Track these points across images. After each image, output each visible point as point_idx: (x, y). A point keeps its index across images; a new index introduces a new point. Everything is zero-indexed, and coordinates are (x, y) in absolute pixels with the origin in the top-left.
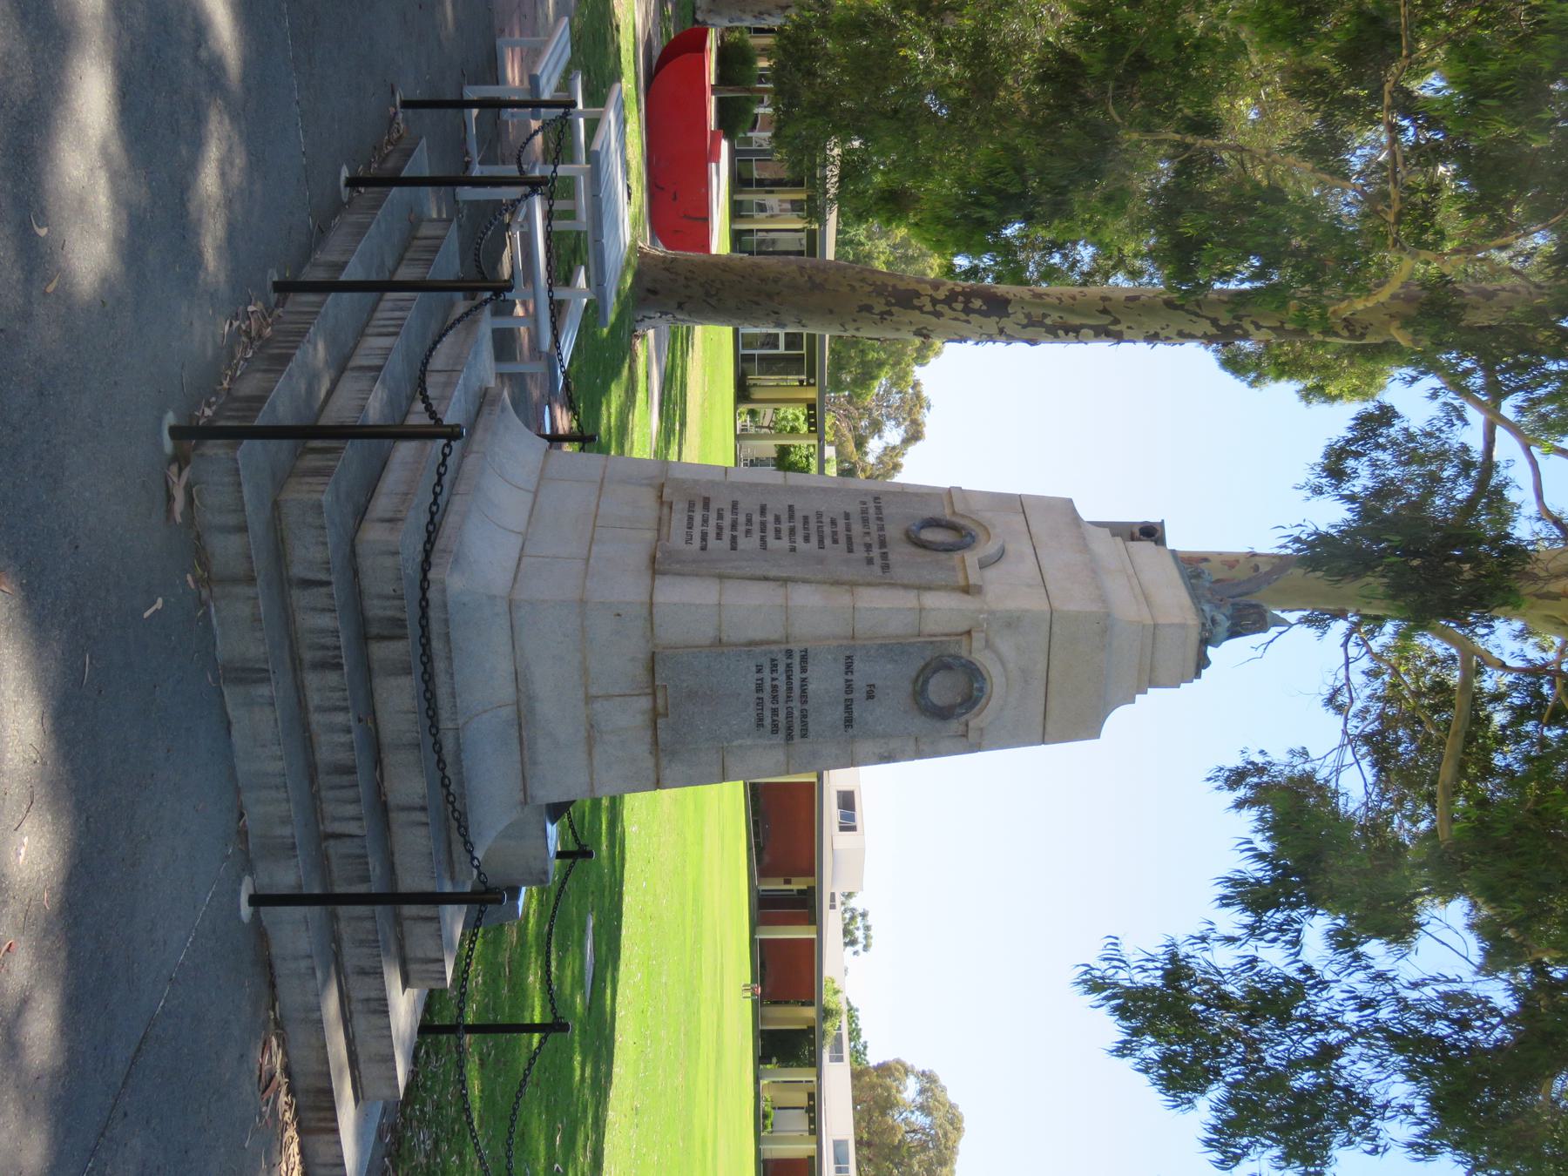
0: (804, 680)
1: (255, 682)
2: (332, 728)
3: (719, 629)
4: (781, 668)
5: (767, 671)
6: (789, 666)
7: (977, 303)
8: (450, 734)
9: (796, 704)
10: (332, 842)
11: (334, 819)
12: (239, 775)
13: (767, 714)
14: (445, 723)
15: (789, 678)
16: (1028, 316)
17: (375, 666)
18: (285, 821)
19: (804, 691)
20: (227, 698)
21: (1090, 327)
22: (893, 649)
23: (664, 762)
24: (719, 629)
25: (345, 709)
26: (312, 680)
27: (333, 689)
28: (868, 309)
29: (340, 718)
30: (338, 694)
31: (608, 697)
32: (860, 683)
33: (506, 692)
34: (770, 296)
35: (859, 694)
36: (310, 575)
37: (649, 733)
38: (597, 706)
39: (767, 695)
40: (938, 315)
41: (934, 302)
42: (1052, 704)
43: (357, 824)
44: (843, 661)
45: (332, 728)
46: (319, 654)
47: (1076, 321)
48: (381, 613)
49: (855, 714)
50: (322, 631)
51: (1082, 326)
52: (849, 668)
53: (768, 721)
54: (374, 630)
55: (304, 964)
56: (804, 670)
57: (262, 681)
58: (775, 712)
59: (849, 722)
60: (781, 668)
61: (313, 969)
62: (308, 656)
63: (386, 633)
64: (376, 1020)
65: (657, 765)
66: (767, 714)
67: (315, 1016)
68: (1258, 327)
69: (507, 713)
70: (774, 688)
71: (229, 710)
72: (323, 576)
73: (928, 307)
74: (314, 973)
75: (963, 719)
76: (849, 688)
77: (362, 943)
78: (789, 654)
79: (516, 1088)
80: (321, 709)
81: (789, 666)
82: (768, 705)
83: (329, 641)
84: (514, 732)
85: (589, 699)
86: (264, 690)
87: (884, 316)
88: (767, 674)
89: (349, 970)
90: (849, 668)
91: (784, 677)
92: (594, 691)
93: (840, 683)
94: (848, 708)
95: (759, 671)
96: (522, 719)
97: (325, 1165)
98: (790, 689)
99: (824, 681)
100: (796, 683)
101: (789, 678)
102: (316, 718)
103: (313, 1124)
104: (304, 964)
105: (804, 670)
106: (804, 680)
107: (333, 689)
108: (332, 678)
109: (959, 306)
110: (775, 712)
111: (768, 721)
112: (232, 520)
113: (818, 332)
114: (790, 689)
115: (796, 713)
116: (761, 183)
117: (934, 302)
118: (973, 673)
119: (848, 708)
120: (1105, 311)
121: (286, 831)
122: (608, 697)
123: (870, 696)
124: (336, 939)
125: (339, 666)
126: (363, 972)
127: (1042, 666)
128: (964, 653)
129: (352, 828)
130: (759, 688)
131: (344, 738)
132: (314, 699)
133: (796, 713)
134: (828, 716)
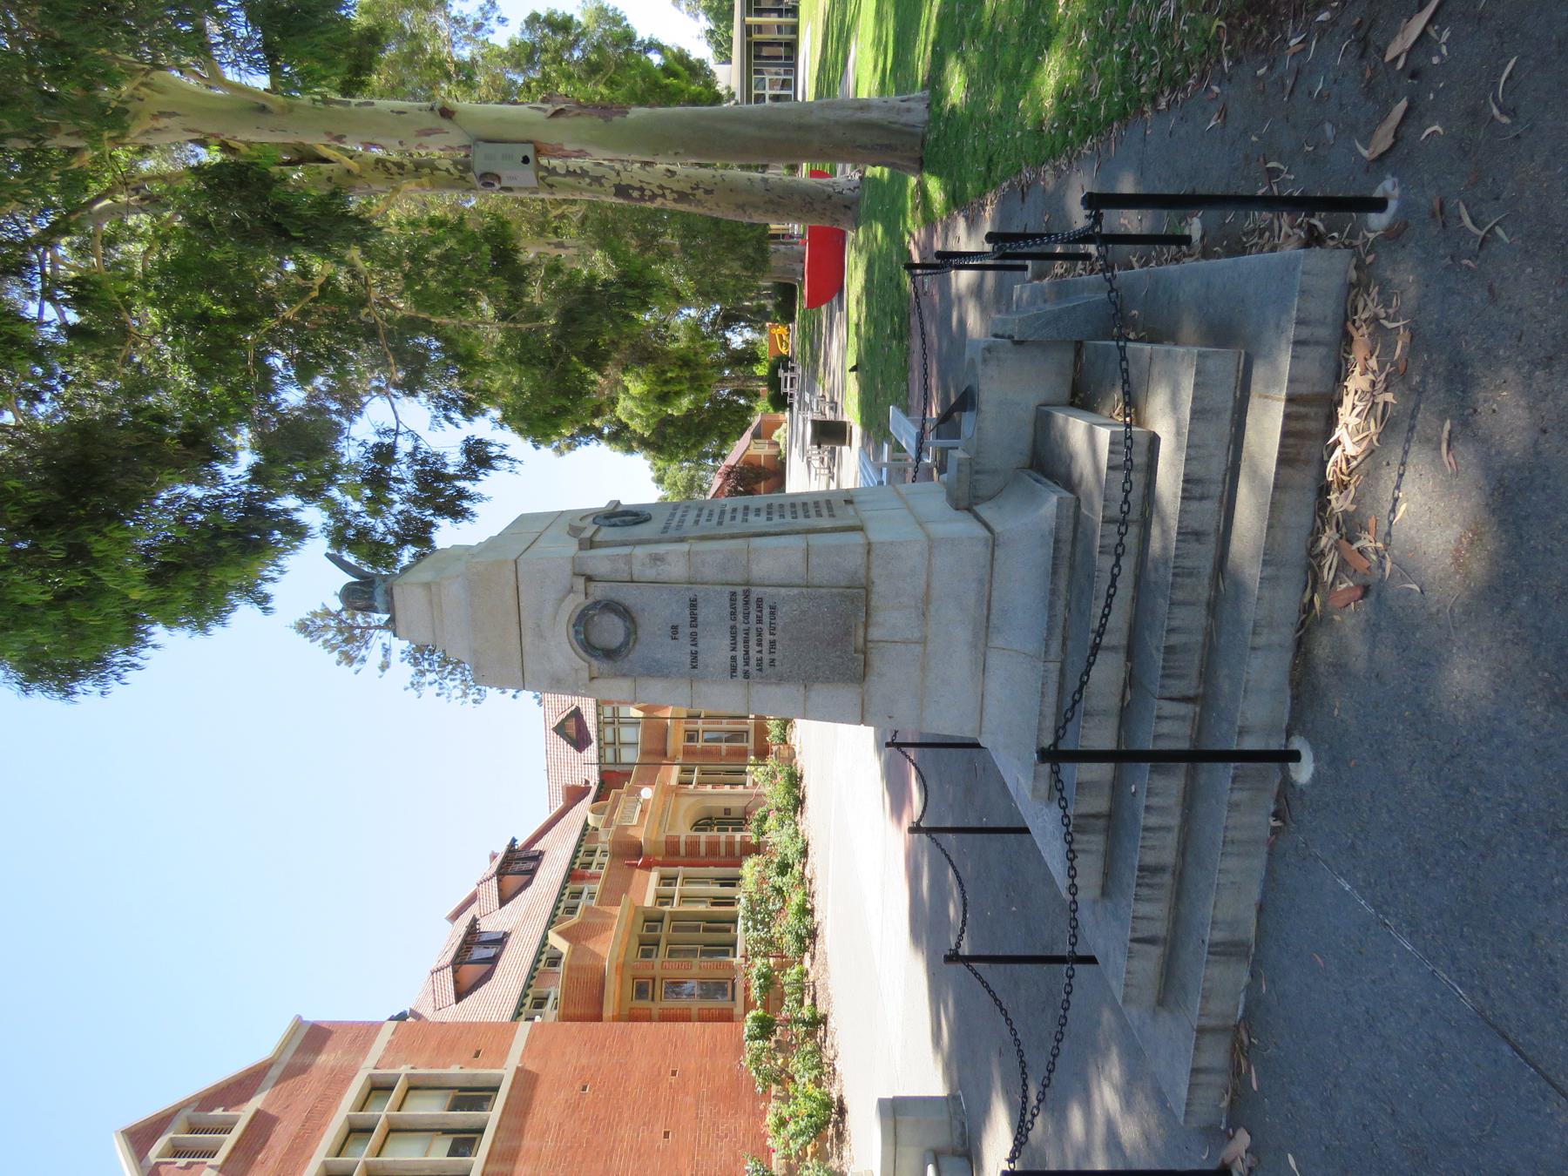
0: (734, 649)
1: (1223, 944)
2: (1161, 810)
3: (806, 699)
4: (753, 662)
5: (766, 662)
6: (747, 664)
7: (636, 194)
8: (1052, 657)
9: (741, 627)
10: (1191, 693)
11: (1183, 718)
12: (1265, 856)
13: (766, 619)
14: (1054, 667)
15: (747, 652)
16: (601, 185)
17: (1107, 790)
18: (1234, 806)
19: (734, 638)
20: (1253, 929)
21: (558, 174)
22: (656, 670)
23: (862, 572)
24: (806, 699)
25: (1146, 829)
26: (1168, 856)
27: (1153, 848)
28: (707, 192)
29: (1153, 821)
30: (1149, 843)
31: (906, 642)
32: (684, 639)
33: (994, 660)
34: (771, 202)
35: (685, 630)
36: (1147, 947)
37: (873, 604)
38: (917, 635)
39: (767, 637)
40: (661, 187)
41: (663, 196)
42: (513, 602)
43: (1164, 713)
44: (700, 665)
45: (1161, 810)
46: (1157, 880)
47: (569, 180)
48: (1093, 838)
49: (687, 612)
50: (1149, 900)
51: (564, 176)
52: (694, 655)
53: (766, 611)
54: (1101, 823)
55: (1261, 641)
56: (734, 658)
57: (1217, 944)
58: (760, 620)
59: (693, 604)
60: (753, 662)
61: (1254, 633)
62: (1167, 879)
63: (1092, 821)
64: (1199, 470)
65: (868, 568)
66: (766, 619)
67: (1270, 571)
68: (447, 170)
69: (997, 641)
70: (760, 644)
71: (1254, 921)
72: (1136, 946)
73: (667, 192)
74: (1255, 626)
75: (590, 600)
76: (694, 638)
77: (1190, 574)
78: (746, 675)
79: (1064, 1045)
80: (1168, 829)
81: (747, 664)
82: (765, 627)
83: (1145, 891)
84: (994, 619)
85: (923, 641)
86: (1219, 936)
87: (697, 187)
88: (766, 657)
89: (1213, 539)
90: (694, 655)
91: (752, 653)
92: (918, 649)
93: (701, 642)
94: (694, 618)
95: (773, 661)
96: (985, 627)
97: (1317, 343)
98: (746, 641)
99: (716, 648)
100: (740, 646)
101: (747, 652)
102: (1174, 821)
103: (1312, 411)
104: (1261, 641)
105: (734, 658)
106: (734, 649)
107: (1153, 848)
108: (1150, 859)
109: (647, 193)
110: (760, 620)
111: (766, 611)
112: (1202, 1078)
113: (745, 106)
114: (746, 641)
115: (740, 617)
116: (780, 44)
117: (663, 196)
118: (589, 647)
119: (694, 618)
120: (551, 186)
121: (1237, 796)
122: (906, 642)
123: (675, 628)
124: (1213, 607)
125: (1141, 869)
126: (1198, 535)
127: (527, 640)
128: (595, 663)
129: (1169, 708)
130: (773, 643)
131: (1154, 801)
132: (1171, 839)
133: (740, 617)
134: (713, 611)
